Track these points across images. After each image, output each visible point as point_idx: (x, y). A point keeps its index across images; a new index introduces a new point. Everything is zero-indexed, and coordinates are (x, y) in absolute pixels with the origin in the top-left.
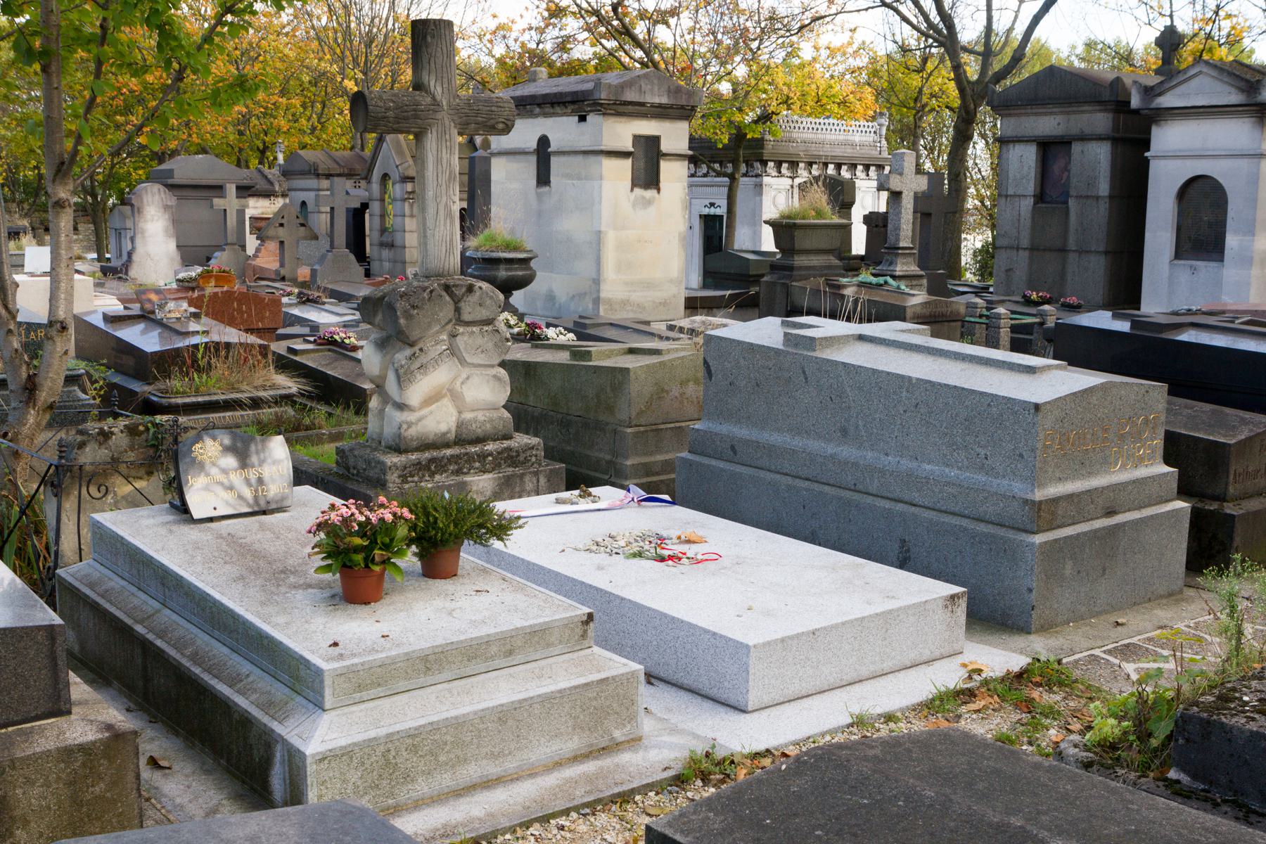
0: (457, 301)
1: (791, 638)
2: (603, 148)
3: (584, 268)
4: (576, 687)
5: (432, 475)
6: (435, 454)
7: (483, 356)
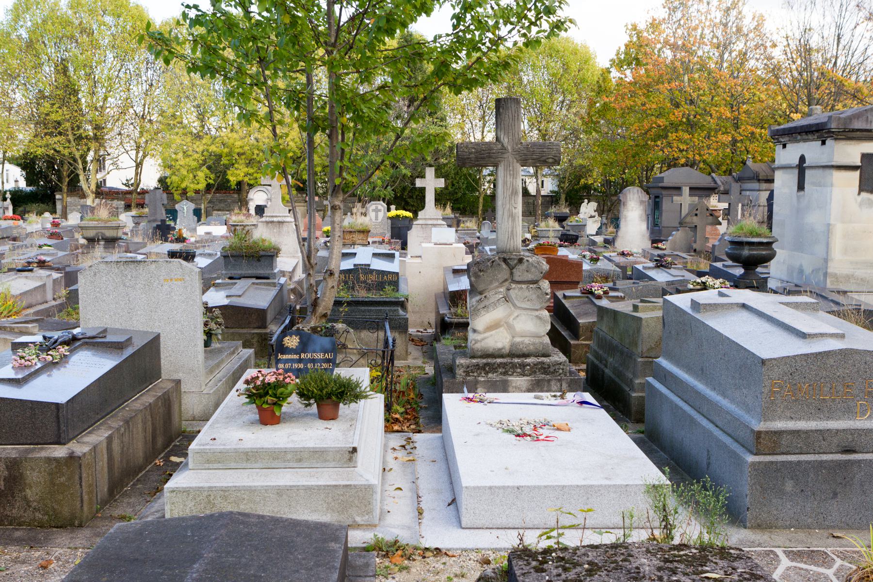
0: (511, 268)
1: (499, 488)
2: (834, 164)
3: (819, 249)
4: (328, 486)
5: (487, 373)
6: (489, 360)
7: (529, 303)
